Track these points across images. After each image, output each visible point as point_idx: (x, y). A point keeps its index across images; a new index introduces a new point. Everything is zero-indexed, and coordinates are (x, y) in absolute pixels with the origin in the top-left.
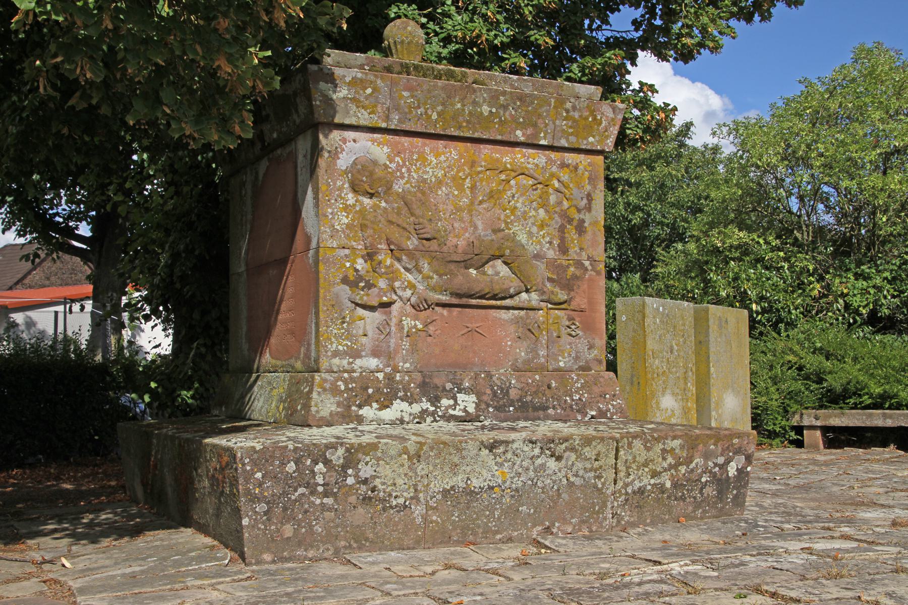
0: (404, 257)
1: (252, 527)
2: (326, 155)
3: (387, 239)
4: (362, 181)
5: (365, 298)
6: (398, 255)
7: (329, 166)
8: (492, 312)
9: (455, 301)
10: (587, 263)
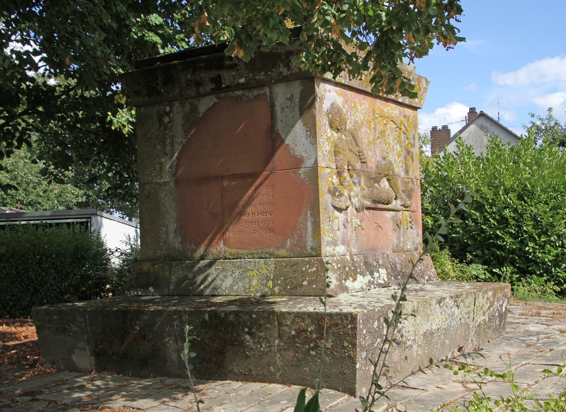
0: (355, 175)
1: (361, 368)
2: (318, 100)
3: (348, 162)
4: (336, 120)
5: (339, 203)
6: (352, 173)
7: (320, 108)
8: (384, 212)
9: (373, 206)
10: (415, 180)
